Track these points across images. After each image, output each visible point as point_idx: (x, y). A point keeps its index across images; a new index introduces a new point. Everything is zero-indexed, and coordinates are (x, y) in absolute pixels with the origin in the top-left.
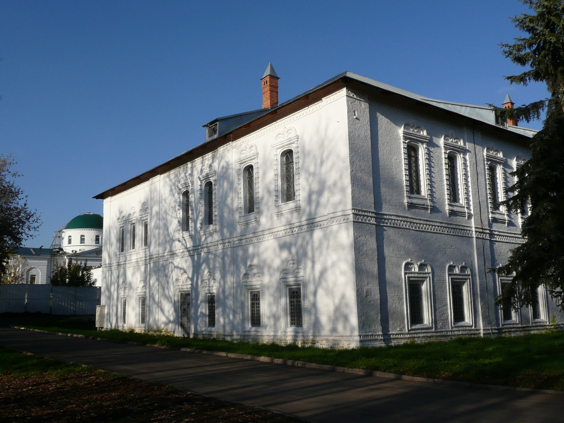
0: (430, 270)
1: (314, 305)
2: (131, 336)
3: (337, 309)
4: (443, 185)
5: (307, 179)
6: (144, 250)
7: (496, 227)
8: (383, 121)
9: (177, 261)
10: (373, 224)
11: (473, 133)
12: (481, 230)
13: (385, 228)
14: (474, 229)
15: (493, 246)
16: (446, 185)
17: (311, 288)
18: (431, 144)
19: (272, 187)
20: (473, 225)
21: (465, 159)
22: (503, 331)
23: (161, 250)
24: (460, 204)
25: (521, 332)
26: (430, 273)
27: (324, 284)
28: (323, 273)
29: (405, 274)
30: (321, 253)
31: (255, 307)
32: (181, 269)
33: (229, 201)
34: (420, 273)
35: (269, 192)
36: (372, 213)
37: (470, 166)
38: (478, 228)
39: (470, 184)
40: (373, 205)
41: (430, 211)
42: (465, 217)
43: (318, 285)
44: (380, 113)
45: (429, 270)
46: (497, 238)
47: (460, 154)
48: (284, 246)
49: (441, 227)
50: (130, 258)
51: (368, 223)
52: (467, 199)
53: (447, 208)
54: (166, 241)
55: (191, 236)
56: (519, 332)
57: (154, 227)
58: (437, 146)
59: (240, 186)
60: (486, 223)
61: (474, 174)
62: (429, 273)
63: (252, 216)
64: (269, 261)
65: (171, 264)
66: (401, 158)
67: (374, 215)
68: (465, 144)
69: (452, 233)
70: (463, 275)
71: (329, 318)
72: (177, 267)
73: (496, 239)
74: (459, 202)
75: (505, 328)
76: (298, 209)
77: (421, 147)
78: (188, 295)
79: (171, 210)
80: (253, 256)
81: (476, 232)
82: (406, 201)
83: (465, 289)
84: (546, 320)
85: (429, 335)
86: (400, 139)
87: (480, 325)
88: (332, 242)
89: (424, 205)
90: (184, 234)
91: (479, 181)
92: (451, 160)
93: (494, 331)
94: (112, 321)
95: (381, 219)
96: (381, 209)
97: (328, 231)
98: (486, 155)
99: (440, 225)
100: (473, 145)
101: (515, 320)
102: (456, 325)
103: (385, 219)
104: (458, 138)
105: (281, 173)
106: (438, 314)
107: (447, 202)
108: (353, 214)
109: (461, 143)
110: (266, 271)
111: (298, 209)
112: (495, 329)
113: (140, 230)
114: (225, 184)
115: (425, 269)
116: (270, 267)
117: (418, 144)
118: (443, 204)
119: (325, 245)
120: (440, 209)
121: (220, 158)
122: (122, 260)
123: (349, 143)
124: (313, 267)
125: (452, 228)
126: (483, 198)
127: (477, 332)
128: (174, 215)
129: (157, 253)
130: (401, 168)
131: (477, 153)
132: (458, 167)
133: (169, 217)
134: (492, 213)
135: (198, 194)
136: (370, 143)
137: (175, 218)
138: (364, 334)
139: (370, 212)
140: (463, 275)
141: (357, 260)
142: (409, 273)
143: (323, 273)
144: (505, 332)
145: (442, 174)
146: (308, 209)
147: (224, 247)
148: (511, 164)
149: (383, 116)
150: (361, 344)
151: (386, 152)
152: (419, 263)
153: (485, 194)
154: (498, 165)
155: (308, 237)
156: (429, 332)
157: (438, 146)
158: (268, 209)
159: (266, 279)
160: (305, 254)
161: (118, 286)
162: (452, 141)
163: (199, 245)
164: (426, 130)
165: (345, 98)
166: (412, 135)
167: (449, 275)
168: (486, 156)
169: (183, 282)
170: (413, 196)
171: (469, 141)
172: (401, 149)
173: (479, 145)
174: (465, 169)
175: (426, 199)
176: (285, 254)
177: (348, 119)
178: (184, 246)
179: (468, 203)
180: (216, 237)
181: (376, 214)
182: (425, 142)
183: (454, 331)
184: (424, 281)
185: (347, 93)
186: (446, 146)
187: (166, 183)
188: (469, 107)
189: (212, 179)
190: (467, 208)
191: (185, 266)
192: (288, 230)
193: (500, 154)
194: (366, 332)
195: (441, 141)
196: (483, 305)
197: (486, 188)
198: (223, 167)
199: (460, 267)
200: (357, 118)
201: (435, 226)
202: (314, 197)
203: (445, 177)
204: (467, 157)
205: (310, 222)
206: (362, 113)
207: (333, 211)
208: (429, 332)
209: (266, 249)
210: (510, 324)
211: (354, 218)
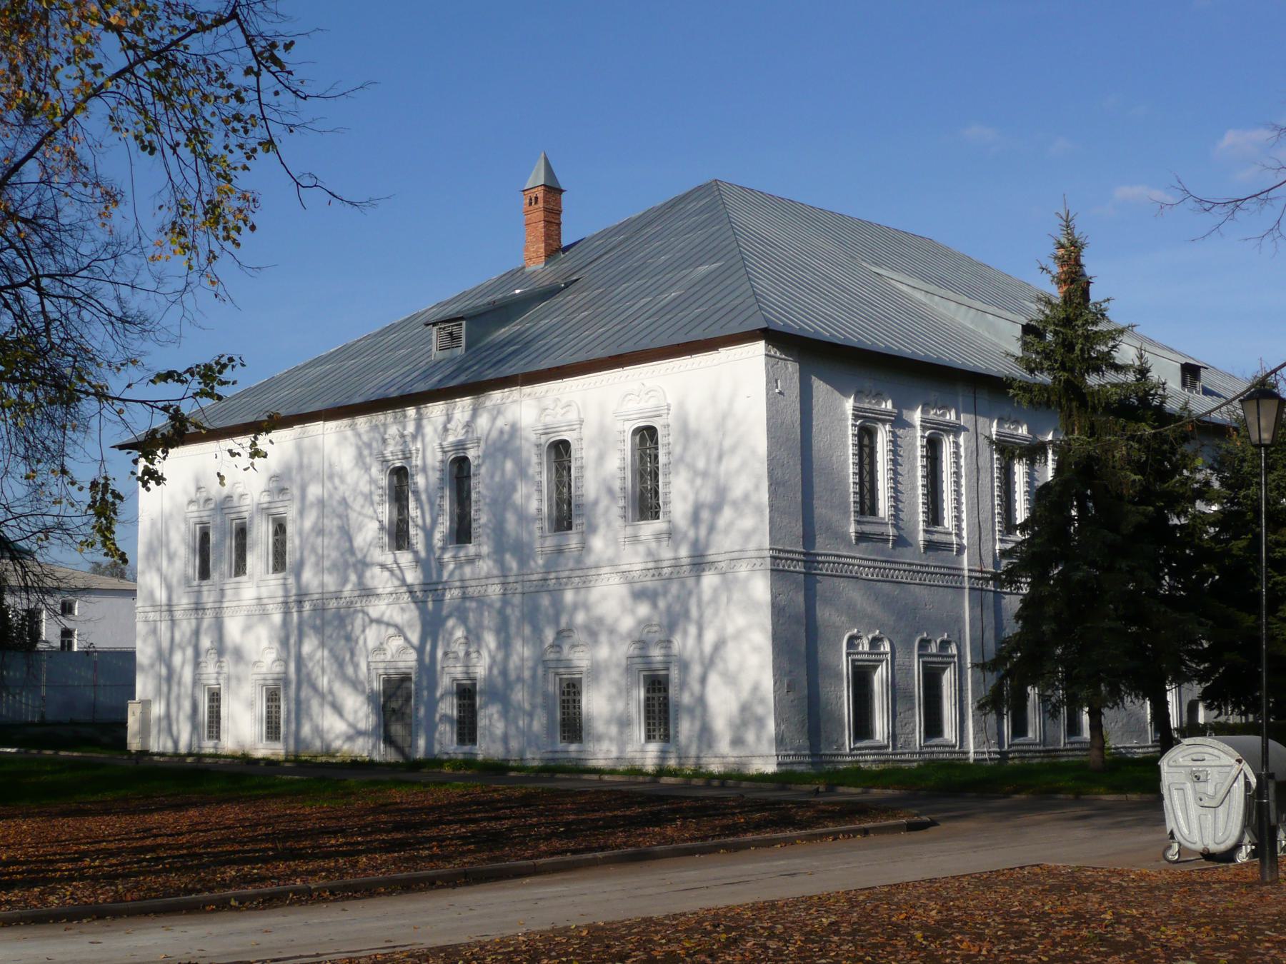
0: (888, 648)
1: (701, 701)
2: (244, 764)
3: (745, 708)
4: (916, 496)
5: (692, 482)
6: (281, 581)
8: (820, 388)
9: (378, 608)
10: (800, 573)
11: (975, 393)
12: (979, 575)
13: (818, 577)
15: (1000, 603)
16: (921, 496)
17: (696, 670)
18: (899, 422)
19: (617, 485)
20: (965, 565)
21: (957, 445)
22: (1011, 756)
23: (331, 582)
27: (720, 666)
28: (719, 645)
29: (848, 654)
30: (716, 613)
31: (571, 707)
32: (388, 624)
33: (518, 497)
34: (872, 654)
35: (610, 491)
36: (800, 553)
38: (975, 571)
39: (963, 490)
43: (709, 664)
44: (820, 379)
45: (886, 647)
47: (948, 437)
48: (639, 595)
49: (909, 571)
50: (237, 594)
51: (793, 572)
52: (958, 518)
53: (921, 536)
54: (346, 565)
55: (418, 561)
57: (313, 529)
58: (909, 425)
59: (541, 472)
60: (989, 561)
62: (886, 653)
63: (573, 540)
64: (609, 620)
65: (360, 615)
67: (802, 557)
68: (958, 417)
69: (927, 582)
70: (943, 657)
72: (379, 621)
74: (943, 525)
75: (1014, 752)
76: (671, 534)
78: (405, 678)
79: (360, 500)
80: (575, 607)
81: (970, 577)
82: (852, 529)
83: (948, 679)
85: (882, 758)
86: (846, 420)
87: (968, 744)
88: (736, 596)
89: (882, 534)
90: (398, 555)
92: (933, 447)
93: (993, 756)
94: (179, 733)
95: (813, 562)
96: (813, 547)
97: (730, 576)
99: (908, 568)
100: (973, 416)
102: (928, 743)
103: (819, 562)
104: (946, 407)
105: (632, 466)
106: (898, 724)
107: (921, 526)
108: (771, 557)
109: (951, 416)
110: (603, 638)
111: (671, 534)
112: (995, 752)
113: (262, 534)
114: (509, 465)
115: (879, 646)
116: (612, 631)
118: (916, 531)
119: (724, 598)
120: (910, 540)
121: (495, 412)
122: (209, 598)
124: (700, 636)
125: (928, 573)
126: (986, 514)
127: (964, 757)
128: (369, 511)
129: (320, 591)
130: (847, 472)
132: (944, 459)
133: (353, 515)
134: (1002, 541)
135: (434, 476)
137: (372, 518)
138: (783, 753)
139: (795, 552)
140: (943, 657)
142: (854, 654)
143: (719, 645)
144: (1013, 758)
145: (915, 476)
146: (691, 534)
147: (505, 589)
152: (870, 637)
153: (990, 507)
155: (691, 582)
156: (883, 754)
157: (911, 426)
158: (609, 525)
159: (603, 652)
160: (686, 614)
161: (197, 653)
162: (936, 414)
163: (438, 583)
165: (762, 360)
167: (920, 656)
169: (393, 656)
170: (865, 519)
171: (966, 411)
172: (847, 437)
173: (983, 415)
174: (957, 463)
175: (886, 524)
176: (643, 610)
178: (398, 579)
179: (959, 527)
180: (485, 566)
181: (805, 554)
182: (889, 421)
183: (924, 753)
184: (877, 667)
185: (766, 349)
187: (345, 438)
189: (471, 454)
190: (956, 535)
191: (399, 618)
192: (652, 572)
195: (917, 416)
197: (993, 496)
198: (501, 432)
199: (938, 641)
200: (780, 393)
201: (899, 570)
202: (705, 515)
203: (920, 482)
204: (961, 440)
205: (697, 560)
207: (737, 548)
208: (883, 754)
209: (604, 598)
210: (1023, 745)
211: (772, 564)
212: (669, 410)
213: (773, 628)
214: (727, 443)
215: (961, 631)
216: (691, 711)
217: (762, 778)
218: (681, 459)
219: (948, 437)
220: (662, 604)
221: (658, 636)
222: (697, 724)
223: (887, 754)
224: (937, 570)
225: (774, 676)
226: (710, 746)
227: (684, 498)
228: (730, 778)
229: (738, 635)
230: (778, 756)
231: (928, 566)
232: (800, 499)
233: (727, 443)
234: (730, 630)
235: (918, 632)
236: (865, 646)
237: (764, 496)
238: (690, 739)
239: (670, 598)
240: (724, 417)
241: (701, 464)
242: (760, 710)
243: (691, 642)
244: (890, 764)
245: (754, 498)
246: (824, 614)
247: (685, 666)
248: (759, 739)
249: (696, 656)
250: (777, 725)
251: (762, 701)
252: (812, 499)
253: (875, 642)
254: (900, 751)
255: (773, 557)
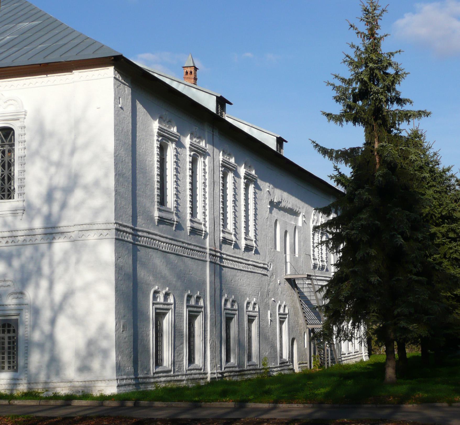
1: (51, 337)
3: (91, 343)
5: (46, 170)
7: (227, 250)
10: (130, 242)
11: (213, 132)
13: (138, 247)
14: (208, 251)
17: (46, 314)
24: (168, 208)
25: (238, 377)
26: (172, 304)
27: (68, 311)
28: (67, 296)
29: (153, 304)
30: (66, 270)
37: (209, 173)
40: (131, 218)
41: (175, 227)
42: (202, 235)
45: (171, 300)
46: (225, 263)
47: (172, 143)
53: (189, 224)
56: (236, 377)
61: (211, 183)
62: (171, 304)
66: (154, 159)
67: (131, 231)
68: (206, 146)
71: (77, 354)
73: (224, 264)
77: (170, 146)
81: (210, 254)
84: (257, 363)
85: (169, 379)
86: (153, 136)
88: (86, 257)
89: (170, 220)
91: (215, 191)
92: (194, 162)
98: (222, 160)
100: (212, 147)
101: (234, 363)
117: (168, 142)
119: (73, 259)
123: (115, 139)
126: (216, 214)
130: (154, 173)
131: (214, 157)
136: (131, 140)
138: (120, 377)
141: (117, 287)
143: (67, 296)
146: (45, 209)
148: (239, 171)
149: (141, 104)
150: (119, 390)
151: (142, 151)
154: (230, 172)
155: (44, 247)
162: (195, 141)
164: (177, 127)
166: (166, 131)
168: (222, 161)
171: (209, 143)
177: (115, 107)
185: (114, 74)
186: (191, 147)
188: (183, 84)
193: (232, 159)
194: (121, 375)
196: (211, 344)
200: (121, 108)
202: (58, 195)
205: (50, 231)
206: (125, 100)
207: (87, 221)
212: (25, 115)
213: (116, 282)
214: (81, 141)
215: (205, 291)
216: (41, 346)
217: (110, 398)
218: (36, 153)
219: (201, 157)
220: (16, 263)
221: (12, 290)
222: (46, 357)
223: (171, 376)
224: (195, 248)
225: (116, 318)
226: (58, 373)
227: (39, 182)
228: (128, 399)
229: (86, 288)
230: (117, 380)
231: (190, 244)
232: (131, 188)
233: (81, 141)
234: (79, 283)
235: (186, 290)
236: (161, 299)
237: (111, 182)
238: (39, 369)
239: (23, 258)
240: (77, 122)
241: (55, 156)
242: (104, 344)
243: (42, 293)
244: (172, 383)
245: (104, 183)
246: (142, 273)
247: (36, 312)
248: (103, 366)
249: (47, 304)
250: (117, 357)
251: (107, 337)
252: (136, 190)
253: (167, 295)
254: (176, 374)
255: (117, 230)
